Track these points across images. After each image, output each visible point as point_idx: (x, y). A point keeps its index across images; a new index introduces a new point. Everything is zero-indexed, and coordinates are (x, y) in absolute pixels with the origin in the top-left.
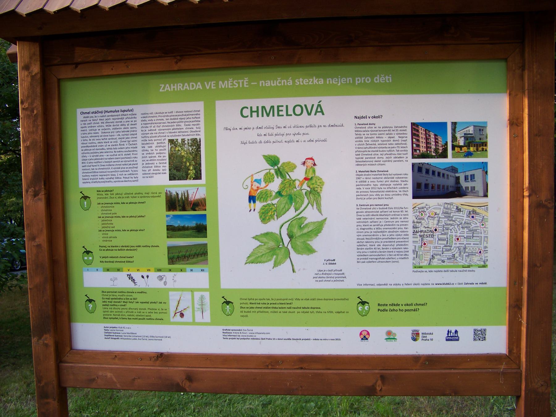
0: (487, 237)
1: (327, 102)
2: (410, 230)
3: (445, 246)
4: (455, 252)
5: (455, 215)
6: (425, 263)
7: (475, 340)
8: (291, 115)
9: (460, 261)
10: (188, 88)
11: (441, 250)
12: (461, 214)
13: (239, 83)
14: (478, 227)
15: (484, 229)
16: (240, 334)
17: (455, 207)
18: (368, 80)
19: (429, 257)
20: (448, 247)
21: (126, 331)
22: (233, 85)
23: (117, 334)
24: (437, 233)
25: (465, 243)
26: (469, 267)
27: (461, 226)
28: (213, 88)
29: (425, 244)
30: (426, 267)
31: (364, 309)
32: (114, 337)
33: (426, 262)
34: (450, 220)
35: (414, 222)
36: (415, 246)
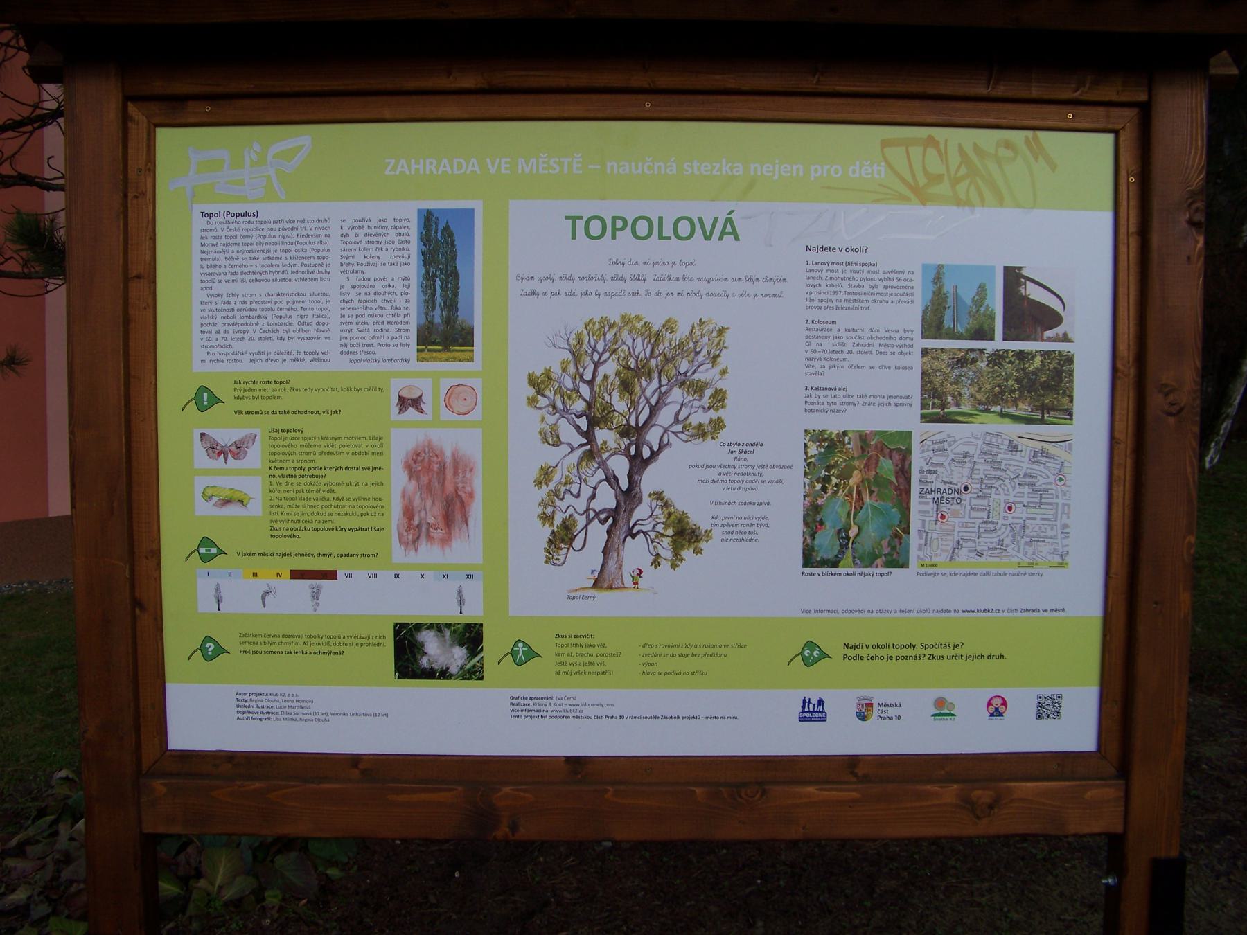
0: (1068, 505)
4: (1004, 533)
5: (1006, 458)
8: (669, 238)
9: (1013, 553)
12: (1018, 456)
16: (548, 707)
19: (951, 544)
23: (265, 710)
25: (1024, 516)
29: (943, 517)
31: (811, 654)
32: (260, 716)
33: (945, 554)
35: (921, 471)
36: (924, 521)
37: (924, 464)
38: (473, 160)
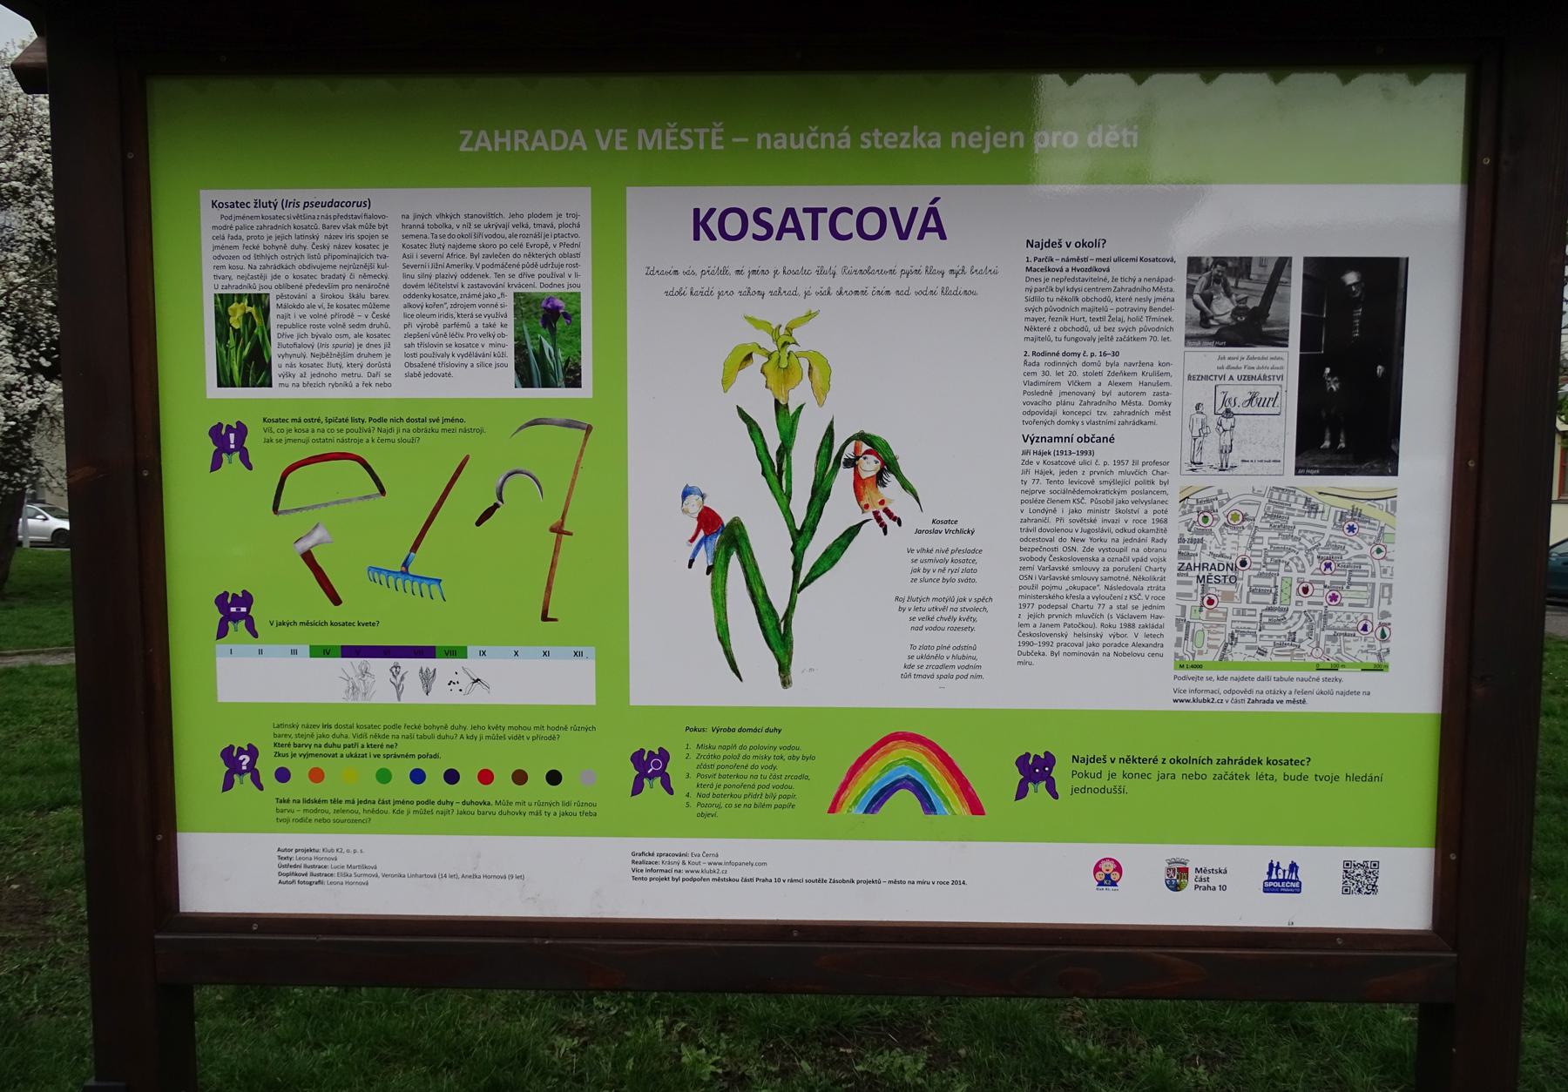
0: (1390, 586)
1: (956, 203)
2: (1173, 562)
3: (1269, 609)
6: (1211, 656)
7: (1346, 891)
8: (806, 210)
9: (1309, 650)
10: (544, 144)
11: (1257, 619)
13: (695, 137)
14: (1364, 557)
15: (1383, 563)
16: (681, 867)
17: (1303, 501)
18: (1070, 140)
19: (1222, 638)
20: (1277, 613)
21: (344, 859)
22: (680, 142)
23: (316, 871)
24: (1247, 573)
26: (1334, 668)
27: (1315, 553)
28: (618, 147)
29: (1211, 602)
30: (1211, 666)
33: (1213, 652)
34: (1287, 538)
35: (1181, 540)
36: (1184, 608)
37: (1184, 530)
38: (578, 132)
